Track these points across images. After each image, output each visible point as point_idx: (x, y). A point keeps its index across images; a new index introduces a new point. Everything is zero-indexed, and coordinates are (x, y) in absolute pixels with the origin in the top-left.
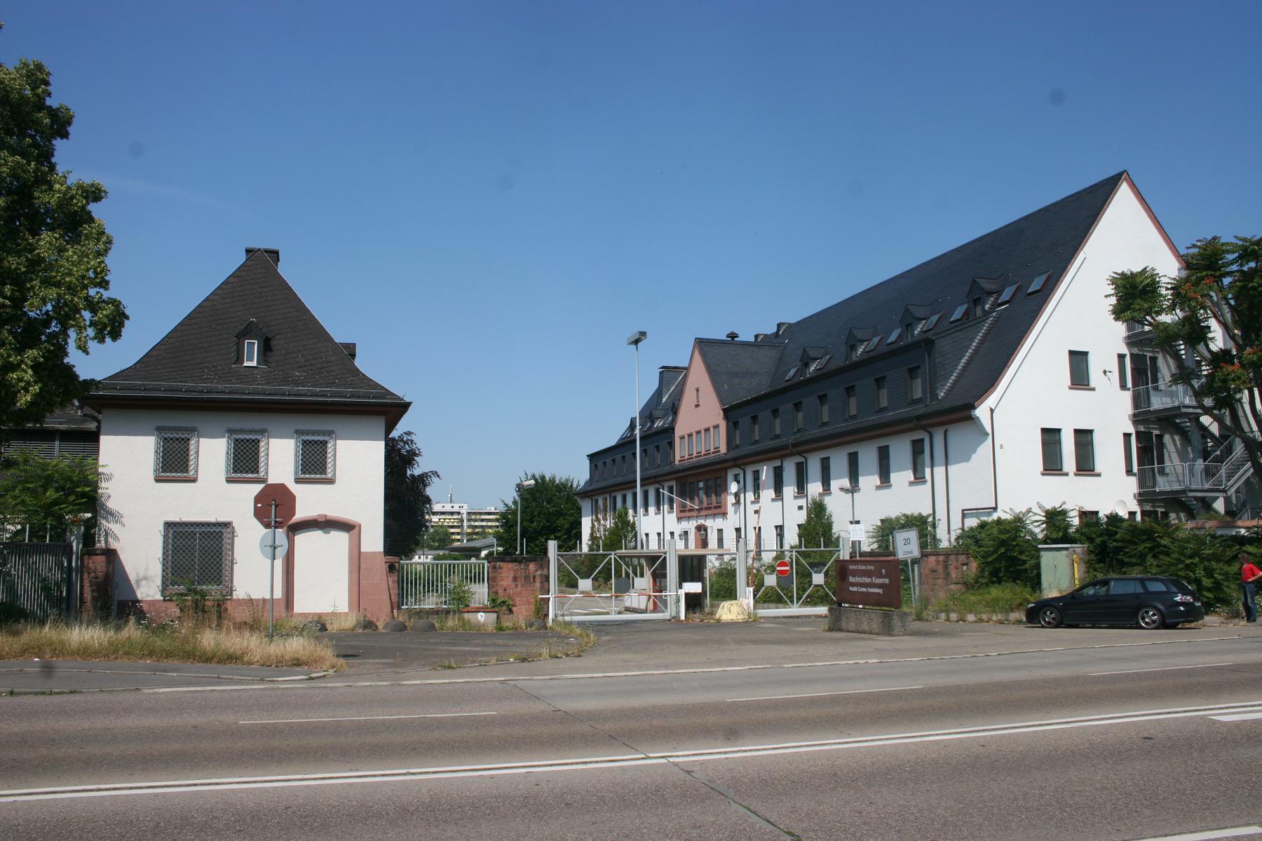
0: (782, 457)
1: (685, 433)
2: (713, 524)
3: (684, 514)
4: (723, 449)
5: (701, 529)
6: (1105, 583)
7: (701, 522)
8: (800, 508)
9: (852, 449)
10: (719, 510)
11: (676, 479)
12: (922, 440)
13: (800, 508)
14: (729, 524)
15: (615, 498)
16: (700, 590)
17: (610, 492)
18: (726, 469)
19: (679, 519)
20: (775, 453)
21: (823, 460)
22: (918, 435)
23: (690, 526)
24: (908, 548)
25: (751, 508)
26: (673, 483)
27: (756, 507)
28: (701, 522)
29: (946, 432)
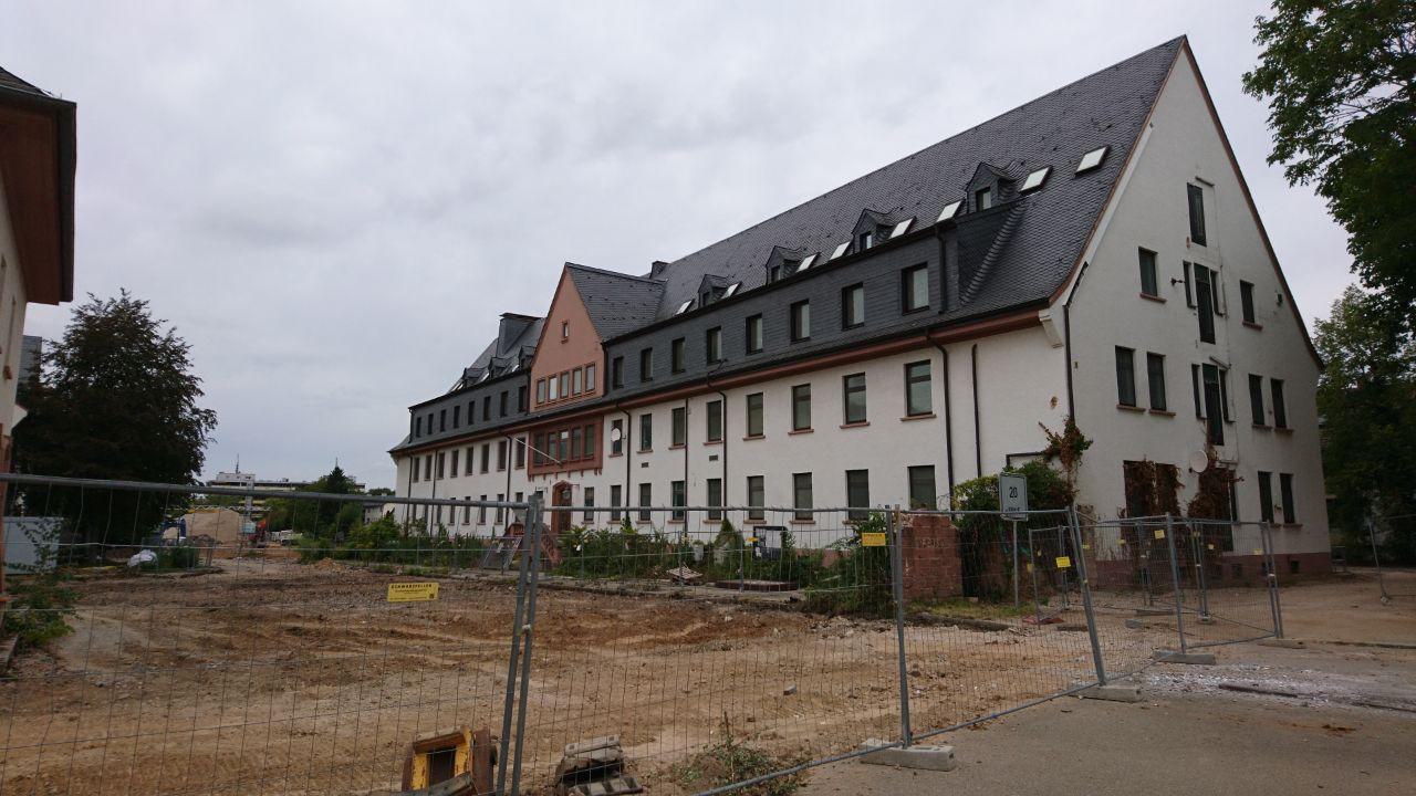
0: (687, 397)
1: (544, 374)
2: (579, 481)
3: (538, 467)
4: (600, 392)
5: (562, 491)
6: (552, 579)
7: (563, 478)
8: (713, 458)
9: (799, 381)
10: (589, 460)
11: (530, 430)
12: (621, 421)
13: (713, 458)
14: (602, 481)
15: (442, 456)
16: (1163, 536)
17: (437, 449)
18: (602, 415)
19: (531, 477)
20: (678, 392)
21: (643, 417)
22: (502, 439)
23: (547, 484)
24: (1014, 503)
25: (637, 460)
26: (526, 436)
27: (645, 458)
28: (563, 478)
29: (975, 347)
